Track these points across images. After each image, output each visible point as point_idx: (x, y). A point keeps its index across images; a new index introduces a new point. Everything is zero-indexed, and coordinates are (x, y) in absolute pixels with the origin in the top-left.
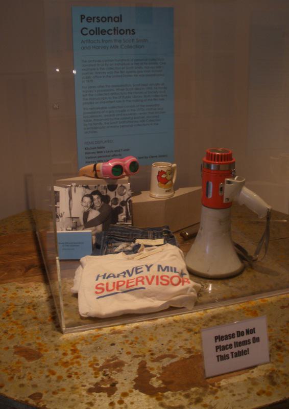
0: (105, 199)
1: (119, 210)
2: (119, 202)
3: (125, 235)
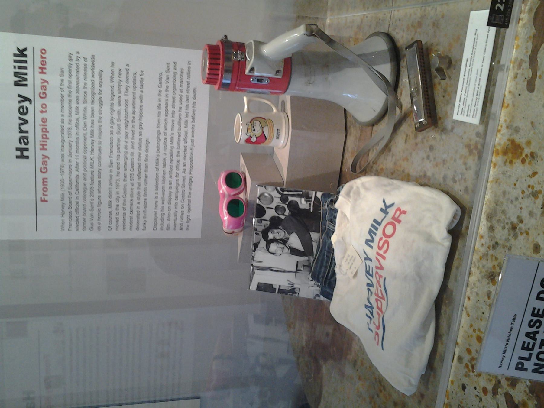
0: (275, 223)
1: (293, 206)
2: (282, 205)
3: (327, 262)
